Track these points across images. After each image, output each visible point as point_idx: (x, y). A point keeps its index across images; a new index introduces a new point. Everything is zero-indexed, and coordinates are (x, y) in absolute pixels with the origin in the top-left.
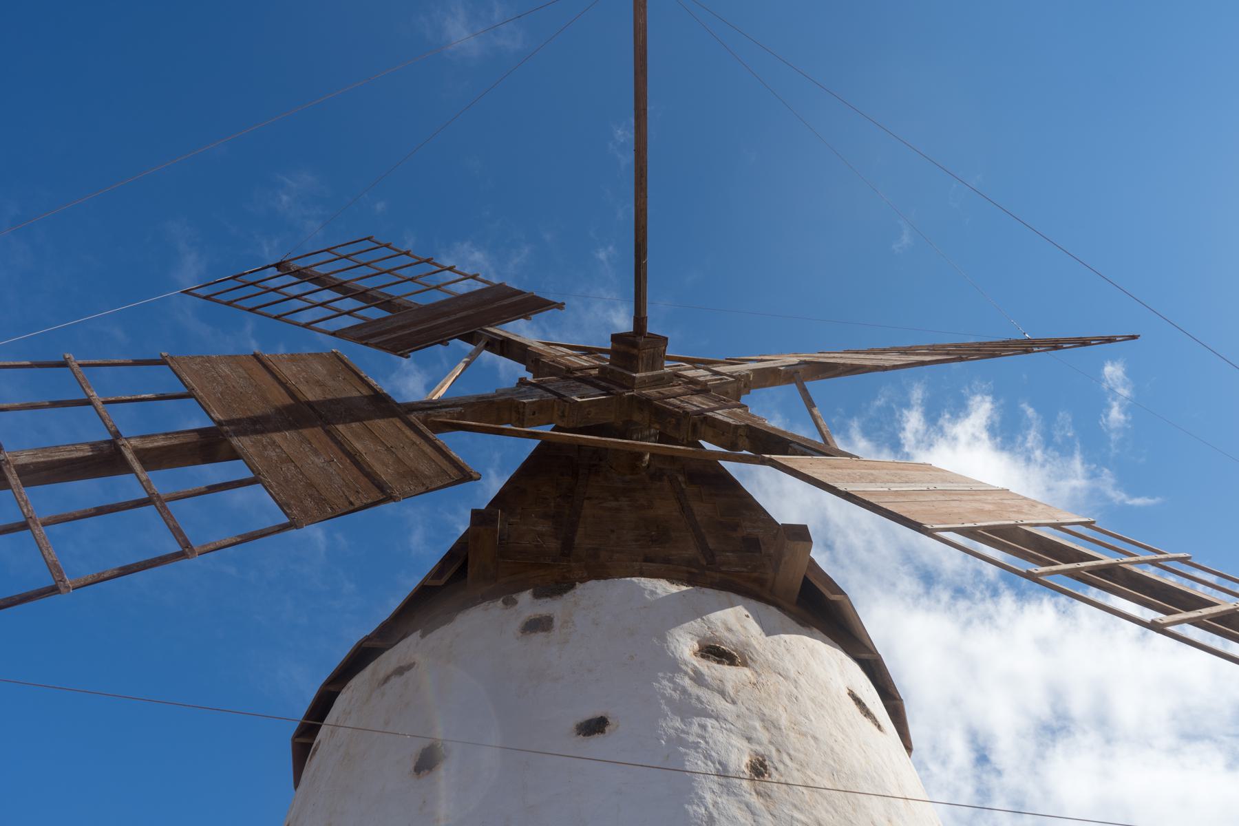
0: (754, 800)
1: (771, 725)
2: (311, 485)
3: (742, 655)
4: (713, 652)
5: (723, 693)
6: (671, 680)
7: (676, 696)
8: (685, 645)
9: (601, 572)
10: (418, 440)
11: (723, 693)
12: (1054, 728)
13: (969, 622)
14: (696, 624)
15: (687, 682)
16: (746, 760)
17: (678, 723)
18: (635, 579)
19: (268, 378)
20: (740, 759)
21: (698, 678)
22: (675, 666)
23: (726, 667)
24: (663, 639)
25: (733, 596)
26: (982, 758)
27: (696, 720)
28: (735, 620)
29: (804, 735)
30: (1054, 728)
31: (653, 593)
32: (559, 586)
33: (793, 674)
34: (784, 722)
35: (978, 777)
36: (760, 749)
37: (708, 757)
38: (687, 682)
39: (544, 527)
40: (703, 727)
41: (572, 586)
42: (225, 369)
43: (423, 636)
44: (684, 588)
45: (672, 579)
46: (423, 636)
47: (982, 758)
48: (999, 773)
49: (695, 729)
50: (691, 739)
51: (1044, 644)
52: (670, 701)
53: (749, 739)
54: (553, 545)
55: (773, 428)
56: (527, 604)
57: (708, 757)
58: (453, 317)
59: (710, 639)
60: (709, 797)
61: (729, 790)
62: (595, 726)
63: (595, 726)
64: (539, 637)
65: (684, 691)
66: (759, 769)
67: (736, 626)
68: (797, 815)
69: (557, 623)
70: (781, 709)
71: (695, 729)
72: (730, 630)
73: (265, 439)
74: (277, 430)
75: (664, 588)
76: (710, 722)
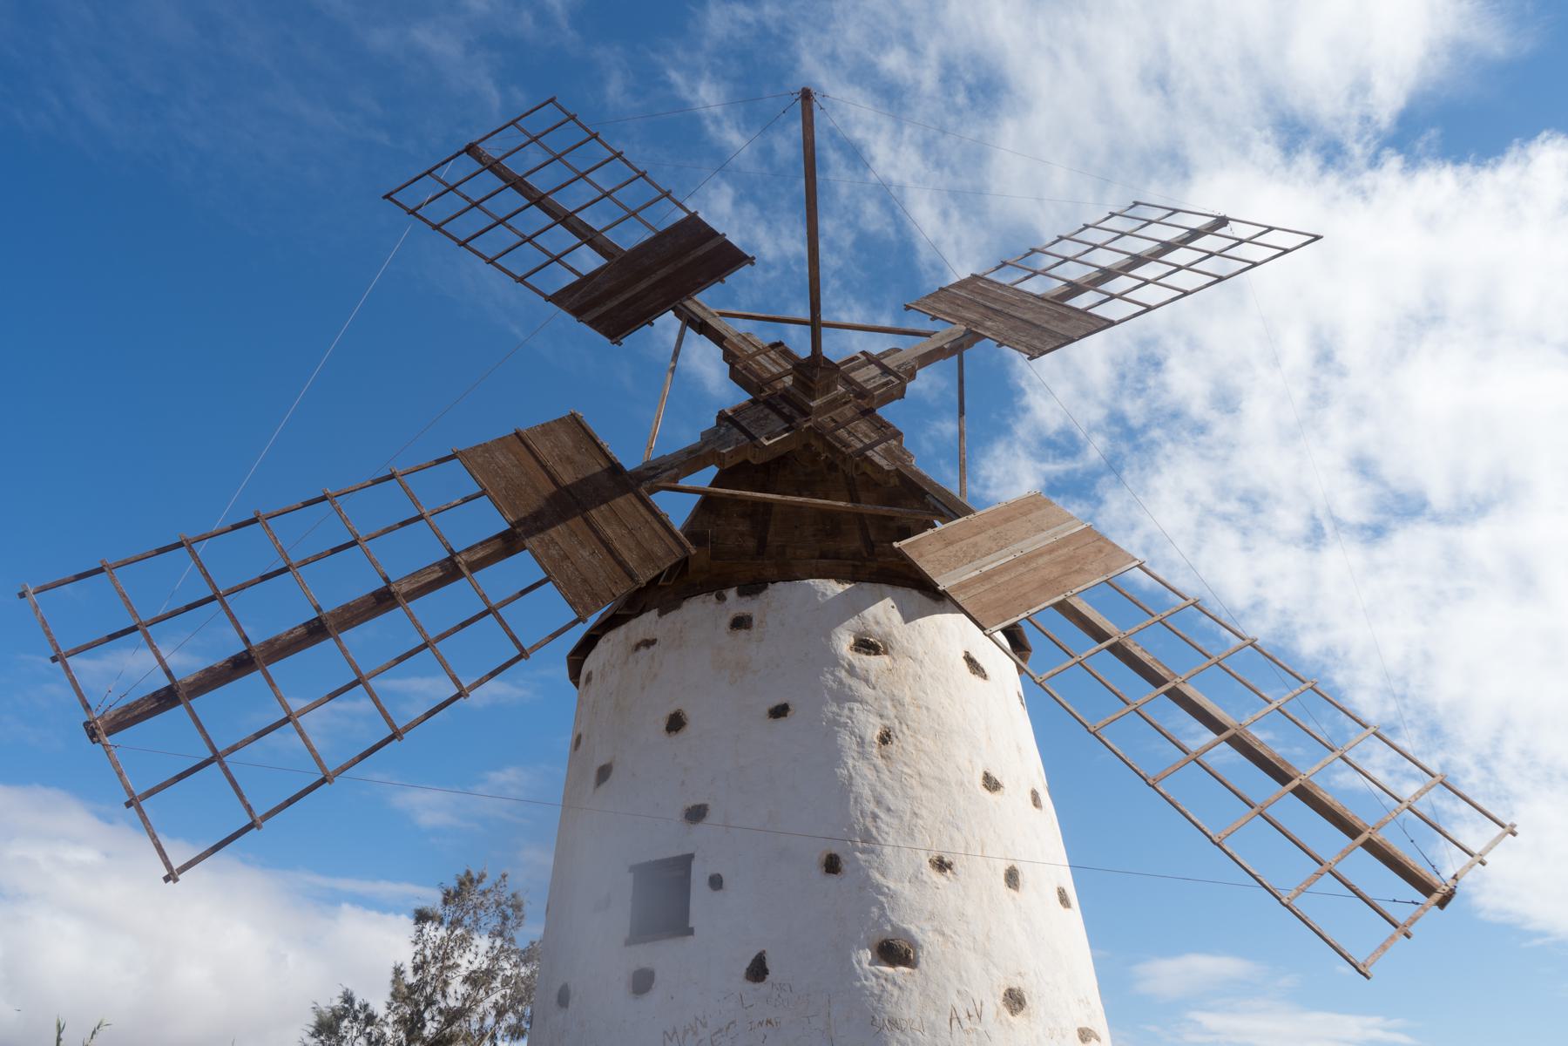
0: (880, 762)
1: (898, 703)
2: (585, 581)
3: (885, 645)
4: (865, 645)
5: (867, 681)
6: (832, 674)
7: (835, 686)
8: (844, 642)
9: (789, 577)
10: (650, 518)
11: (867, 681)
12: (1424, 321)
13: (1336, 198)
14: (853, 622)
15: (843, 674)
16: (877, 733)
17: (835, 709)
18: (811, 581)
19: (532, 460)
20: (873, 734)
21: (851, 670)
22: (835, 661)
23: (872, 658)
24: (829, 638)
25: (884, 586)
26: (1325, 357)
27: (847, 705)
28: (883, 612)
29: (919, 707)
30: (1424, 321)
31: (824, 594)
32: (753, 587)
33: (920, 655)
34: (907, 700)
35: (1315, 380)
36: (888, 723)
37: (852, 733)
38: (843, 674)
39: (743, 527)
40: (851, 710)
41: (765, 587)
42: (501, 458)
43: (660, 615)
44: (848, 586)
45: (840, 579)
46: (660, 615)
47: (1325, 357)
48: (1342, 373)
49: (846, 712)
50: (843, 720)
51: (1430, 222)
52: (830, 690)
53: (881, 716)
54: (751, 544)
55: (917, 473)
56: (734, 603)
57: (852, 733)
58: (655, 278)
59: (863, 634)
60: (850, 762)
61: (863, 755)
62: (780, 712)
63: (780, 712)
64: (742, 633)
65: (841, 682)
66: (885, 738)
67: (883, 620)
68: (906, 770)
69: (755, 622)
70: (906, 690)
71: (846, 712)
72: (878, 623)
73: (545, 536)
74: (552, 525)
75: (833, 588)
76: (856, 706)
